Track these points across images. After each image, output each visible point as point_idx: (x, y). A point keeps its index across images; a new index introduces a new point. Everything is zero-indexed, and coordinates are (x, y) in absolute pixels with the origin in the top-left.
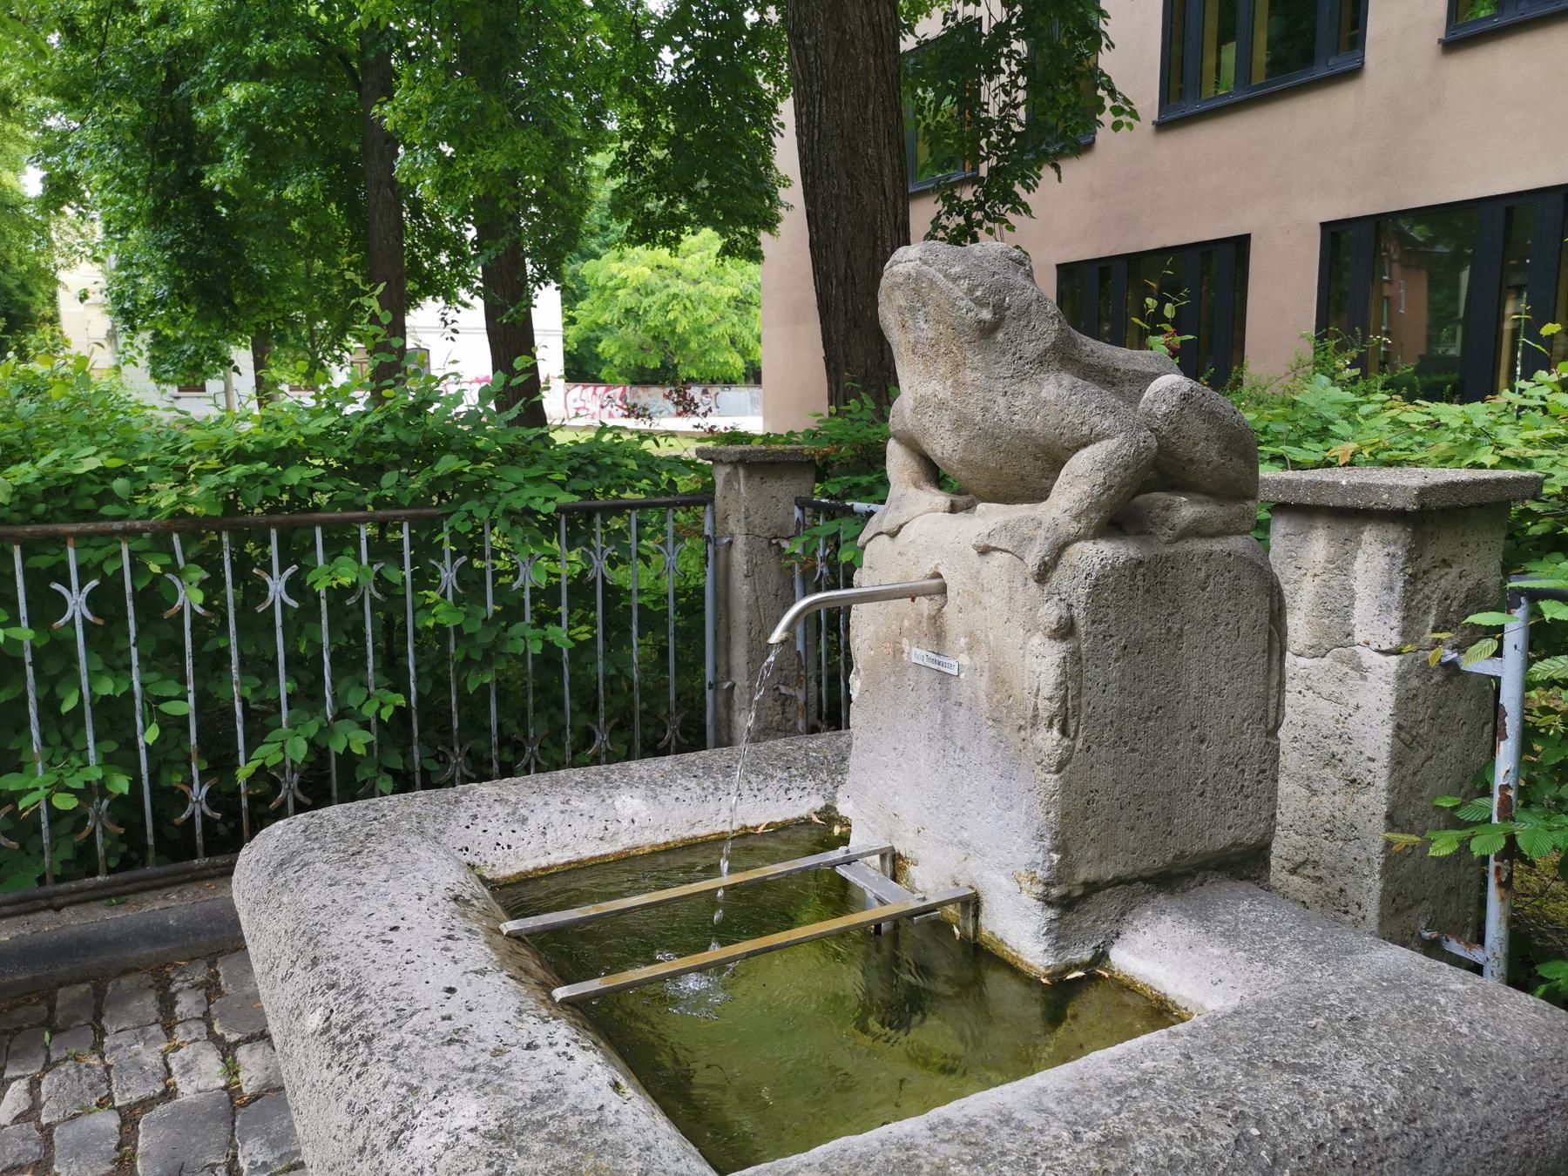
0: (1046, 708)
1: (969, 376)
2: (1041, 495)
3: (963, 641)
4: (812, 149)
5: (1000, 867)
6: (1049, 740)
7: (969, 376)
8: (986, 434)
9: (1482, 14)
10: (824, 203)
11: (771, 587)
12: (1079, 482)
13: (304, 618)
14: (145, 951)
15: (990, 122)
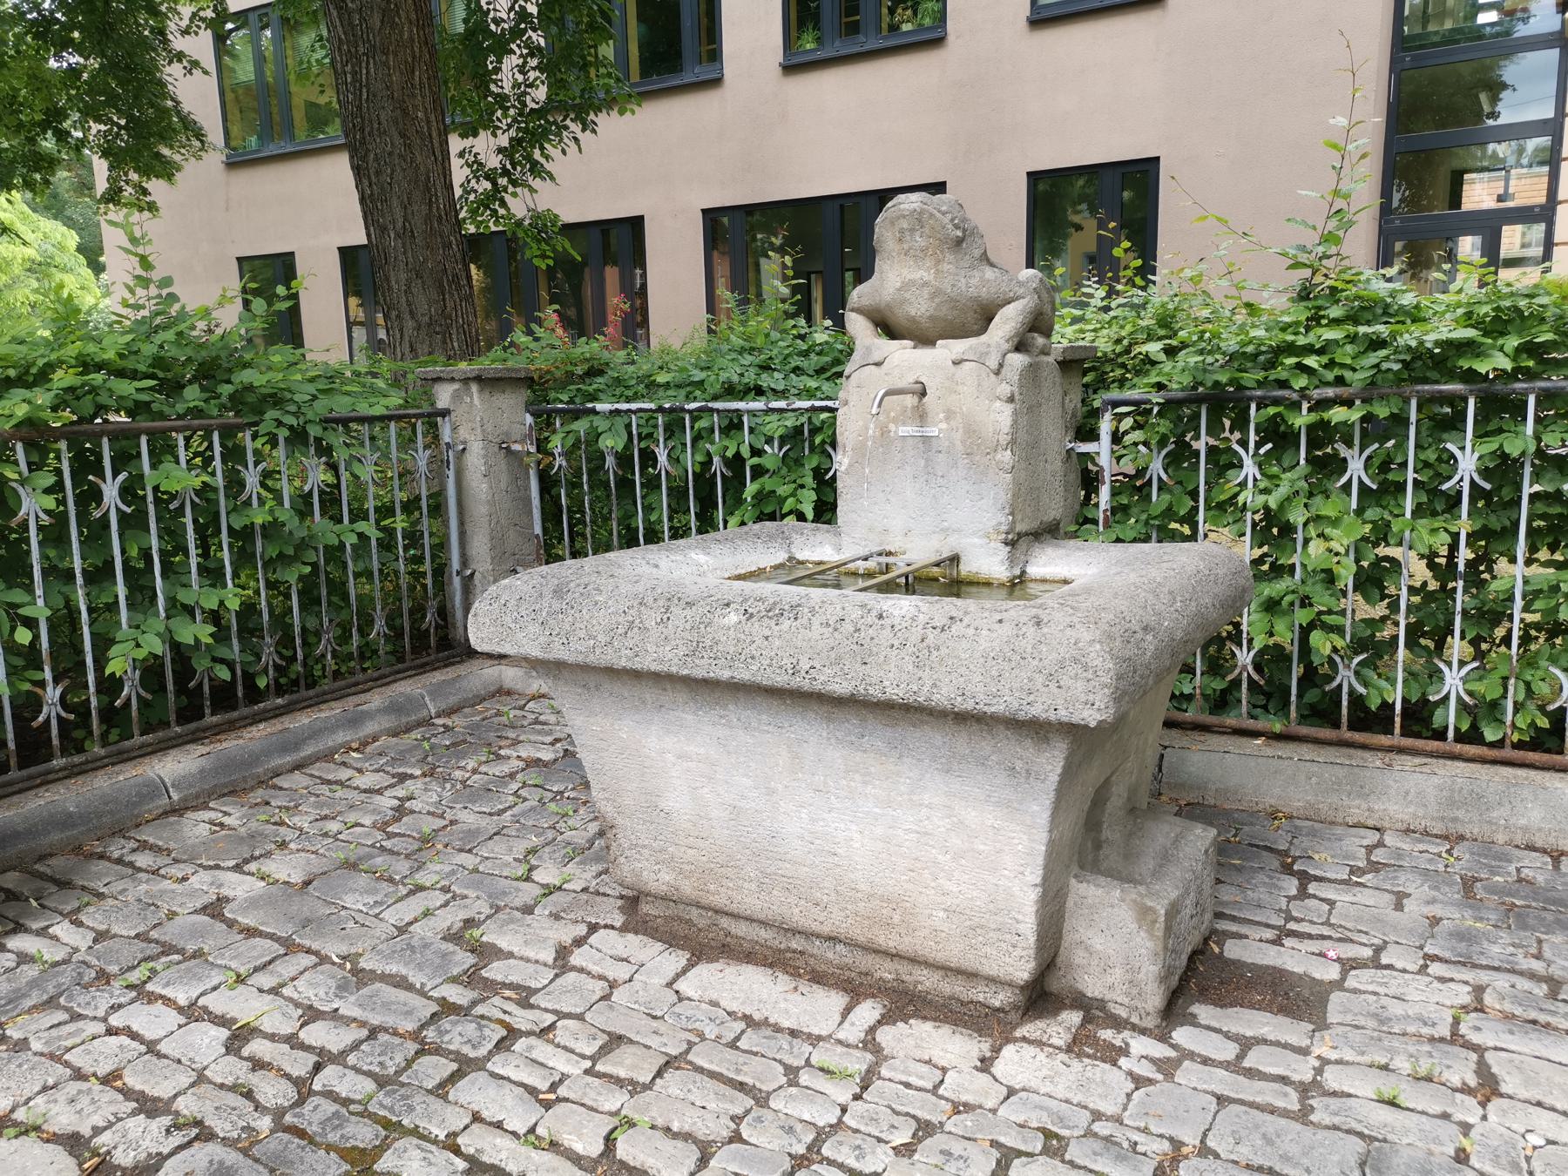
0: (1004, 439)
1: (946, 267)
2: (983, 330)
3: (942, 416)
4: (360, 107)
5: (974, 533)
6: (1006, 457)
7: (946, 267)
8: (952, 300)
9: (808, 46)
10: (376, 159)
11: (503, 485)
12: (1007, 322)
13: (133, 523)
14: (56, 837)
15: (502, 99)
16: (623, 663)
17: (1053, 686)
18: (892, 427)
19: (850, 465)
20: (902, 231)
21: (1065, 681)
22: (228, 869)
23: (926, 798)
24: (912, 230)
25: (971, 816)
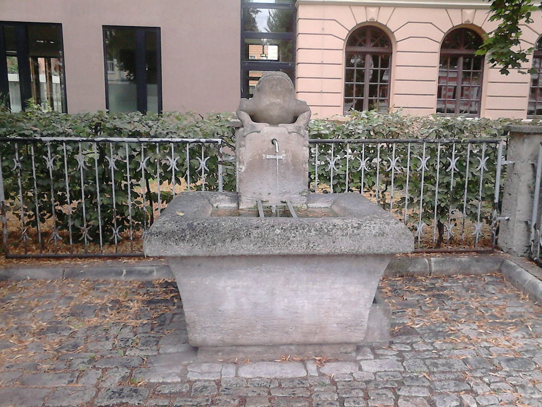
3: (284, 151)
16: (230, 253)
17: (398, 242)
18: (264, 155)
19: (246, 170)
20: (273, 85)
21: (402, 240)
22: (297, 361)
23: (336, 286)
24: (277, 85)
25: (351, 289)
